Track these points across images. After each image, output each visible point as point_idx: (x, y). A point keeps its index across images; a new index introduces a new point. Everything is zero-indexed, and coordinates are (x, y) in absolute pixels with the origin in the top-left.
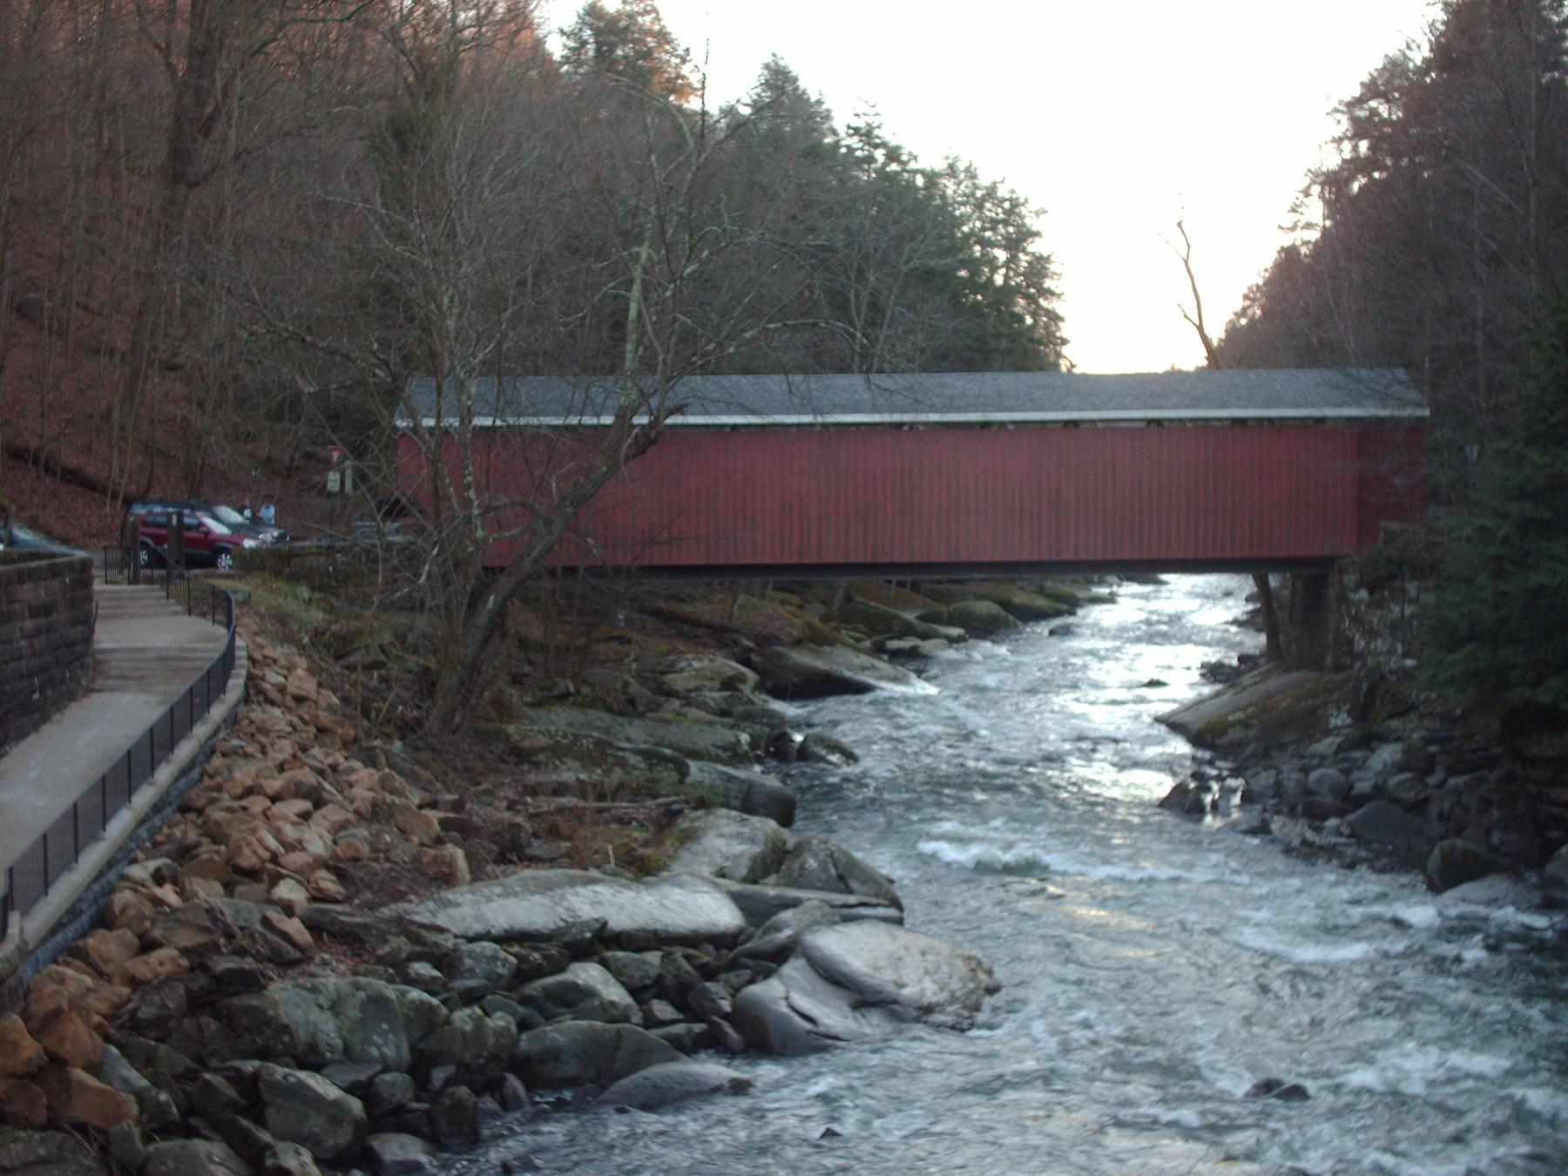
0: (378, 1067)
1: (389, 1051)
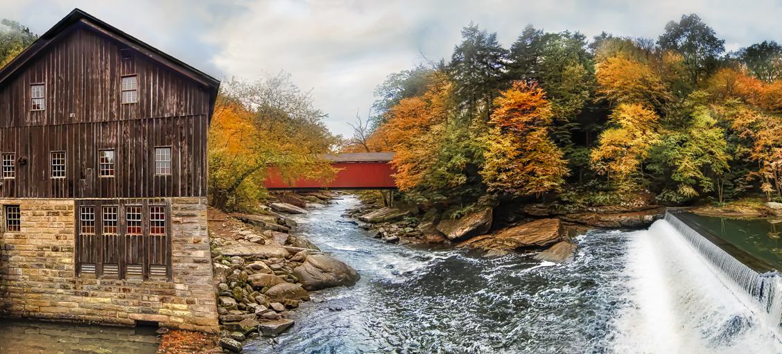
0: (219, 282)
1: (222, 278)
